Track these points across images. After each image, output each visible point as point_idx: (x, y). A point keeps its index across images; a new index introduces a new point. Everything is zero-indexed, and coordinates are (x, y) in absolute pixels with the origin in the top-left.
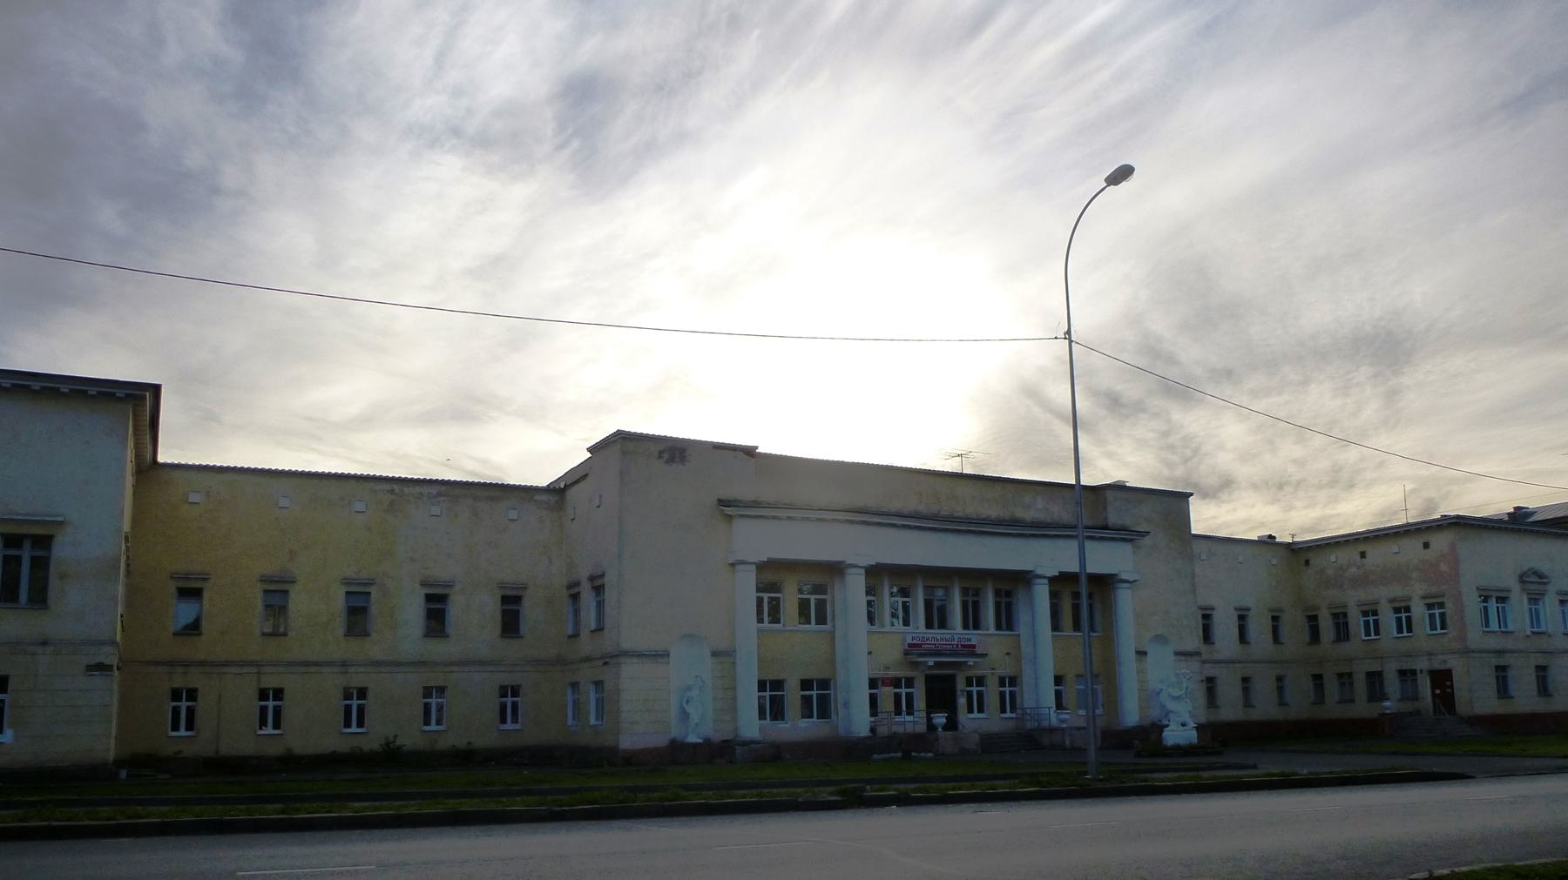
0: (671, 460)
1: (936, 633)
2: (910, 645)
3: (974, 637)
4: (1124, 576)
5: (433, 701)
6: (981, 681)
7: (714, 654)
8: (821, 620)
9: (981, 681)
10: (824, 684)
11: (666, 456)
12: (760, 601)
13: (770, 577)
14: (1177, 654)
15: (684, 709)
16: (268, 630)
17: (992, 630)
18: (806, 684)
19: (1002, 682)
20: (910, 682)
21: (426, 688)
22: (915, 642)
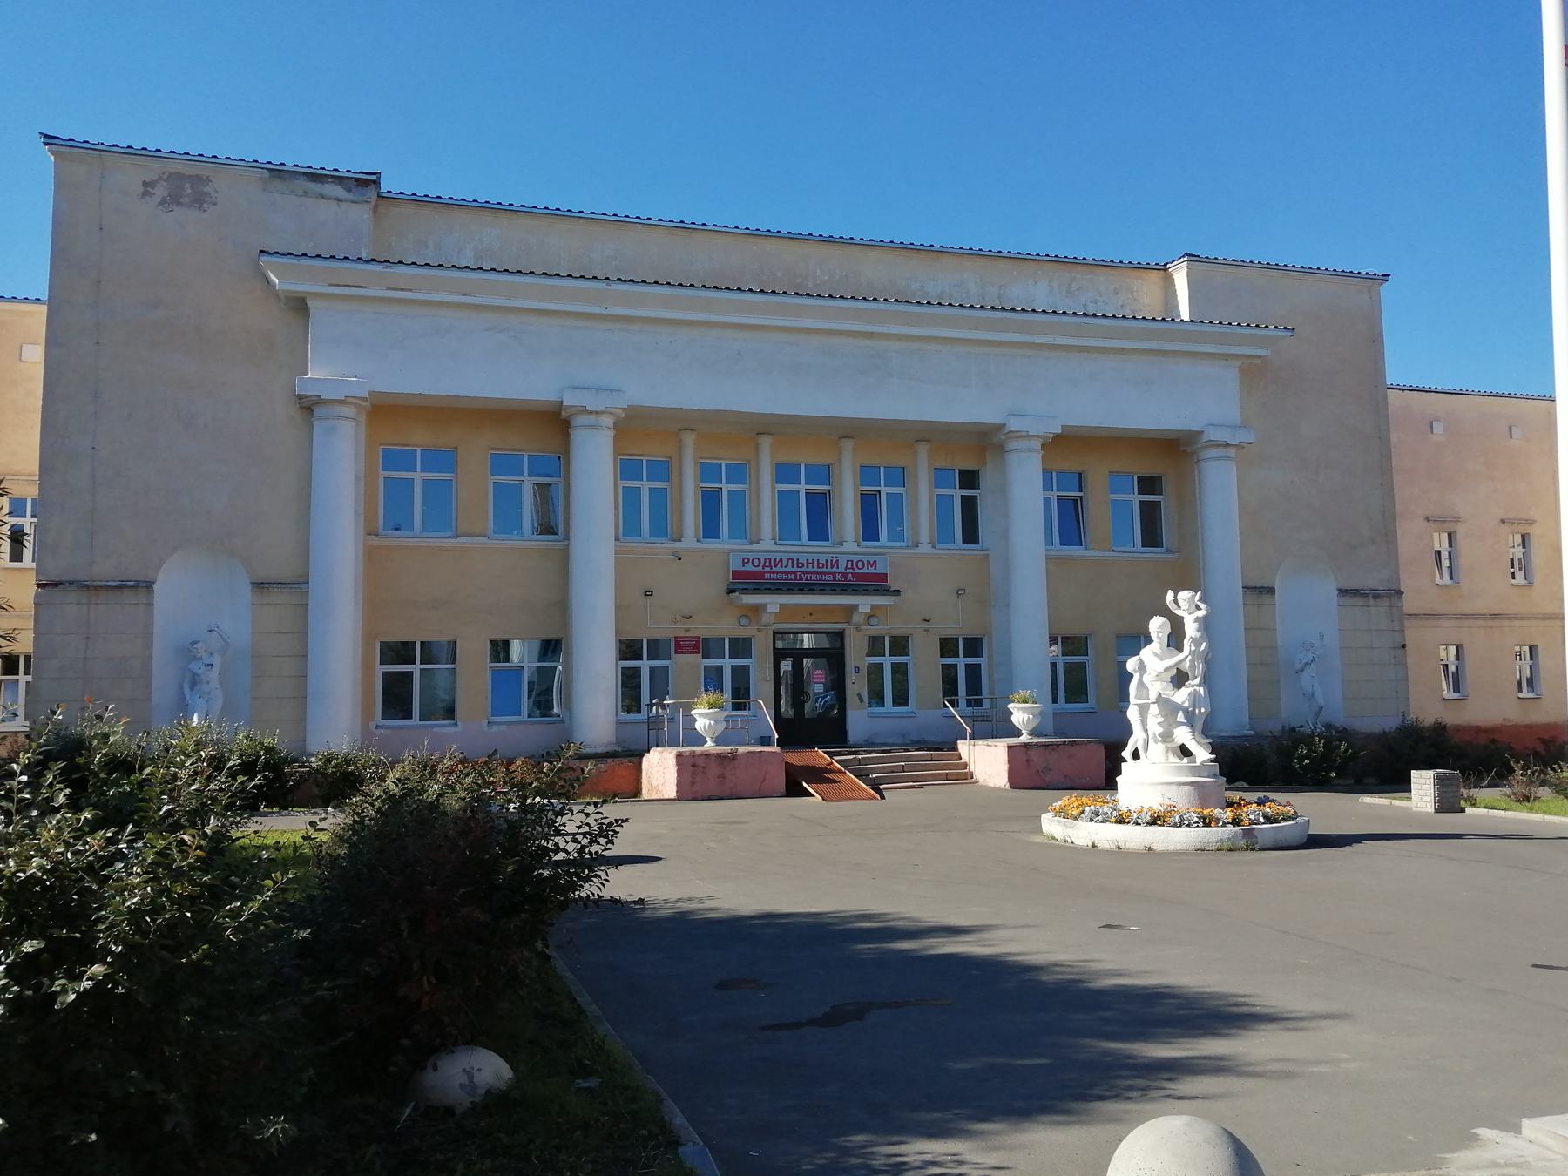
0: (173, 200)
1: (818, 546)
2: (736, 574)
3: (886, 553)
4: (1213, 435)
5: (645, 665)
6: (900, 645)
7: (260, 586)
8: (547, 529)
9: (900, 645)
10: (974, 646)
11: (160, 192)
12: (1047, 501)
13: (1071, 464)
14: (1343, 592)
15: (184, 698)
16: (820, 562)
17: (925, 548)
18: (947, 647)
19: (947, 647)
20: (741, 647)
21: (493, 643)
22: (749, 567)
